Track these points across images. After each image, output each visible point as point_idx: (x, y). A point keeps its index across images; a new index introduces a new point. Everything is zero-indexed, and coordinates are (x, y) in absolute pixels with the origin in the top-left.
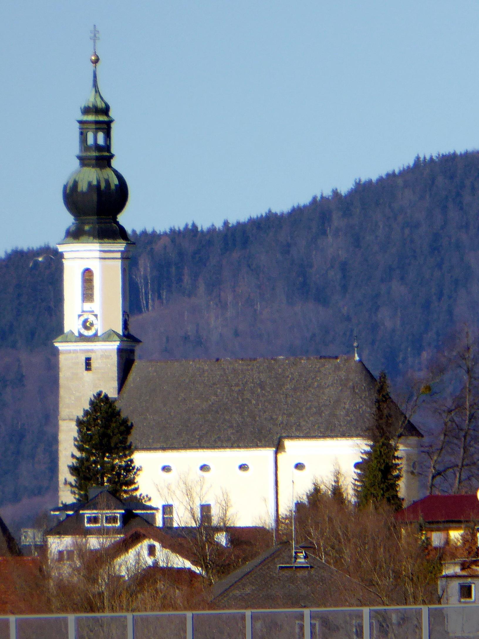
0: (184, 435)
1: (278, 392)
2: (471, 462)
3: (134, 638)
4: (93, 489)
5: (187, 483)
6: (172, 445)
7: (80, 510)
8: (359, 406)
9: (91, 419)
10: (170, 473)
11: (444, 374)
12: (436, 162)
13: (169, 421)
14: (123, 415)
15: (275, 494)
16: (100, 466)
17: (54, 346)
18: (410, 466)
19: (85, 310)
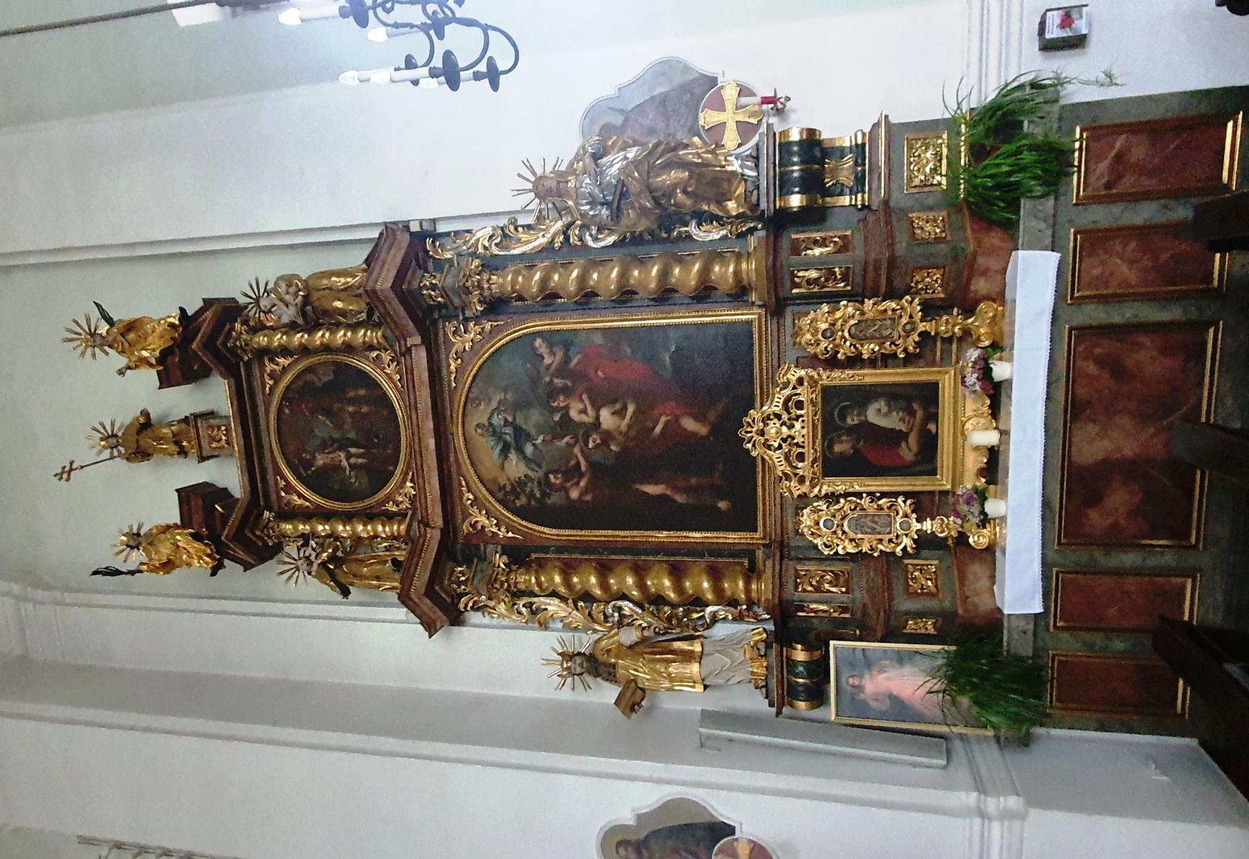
0: (1175, 215)
1: (480, 334)
2: (1046, 135)
3: (6, 34)
4: (557, 494)
5: (358, 299)
6: (311, 328)
7: (703, 437)
8: (732, 227)
9: (411, 254)
10: (359, 28)
11: (171, 338)
12: (635, 482)
13: (1217, 577)
14: (188, 415)
15: (346, 246)
16: (722, 499)
17: (350, 4)
18: (1102, 85)
19: (205, 454)
